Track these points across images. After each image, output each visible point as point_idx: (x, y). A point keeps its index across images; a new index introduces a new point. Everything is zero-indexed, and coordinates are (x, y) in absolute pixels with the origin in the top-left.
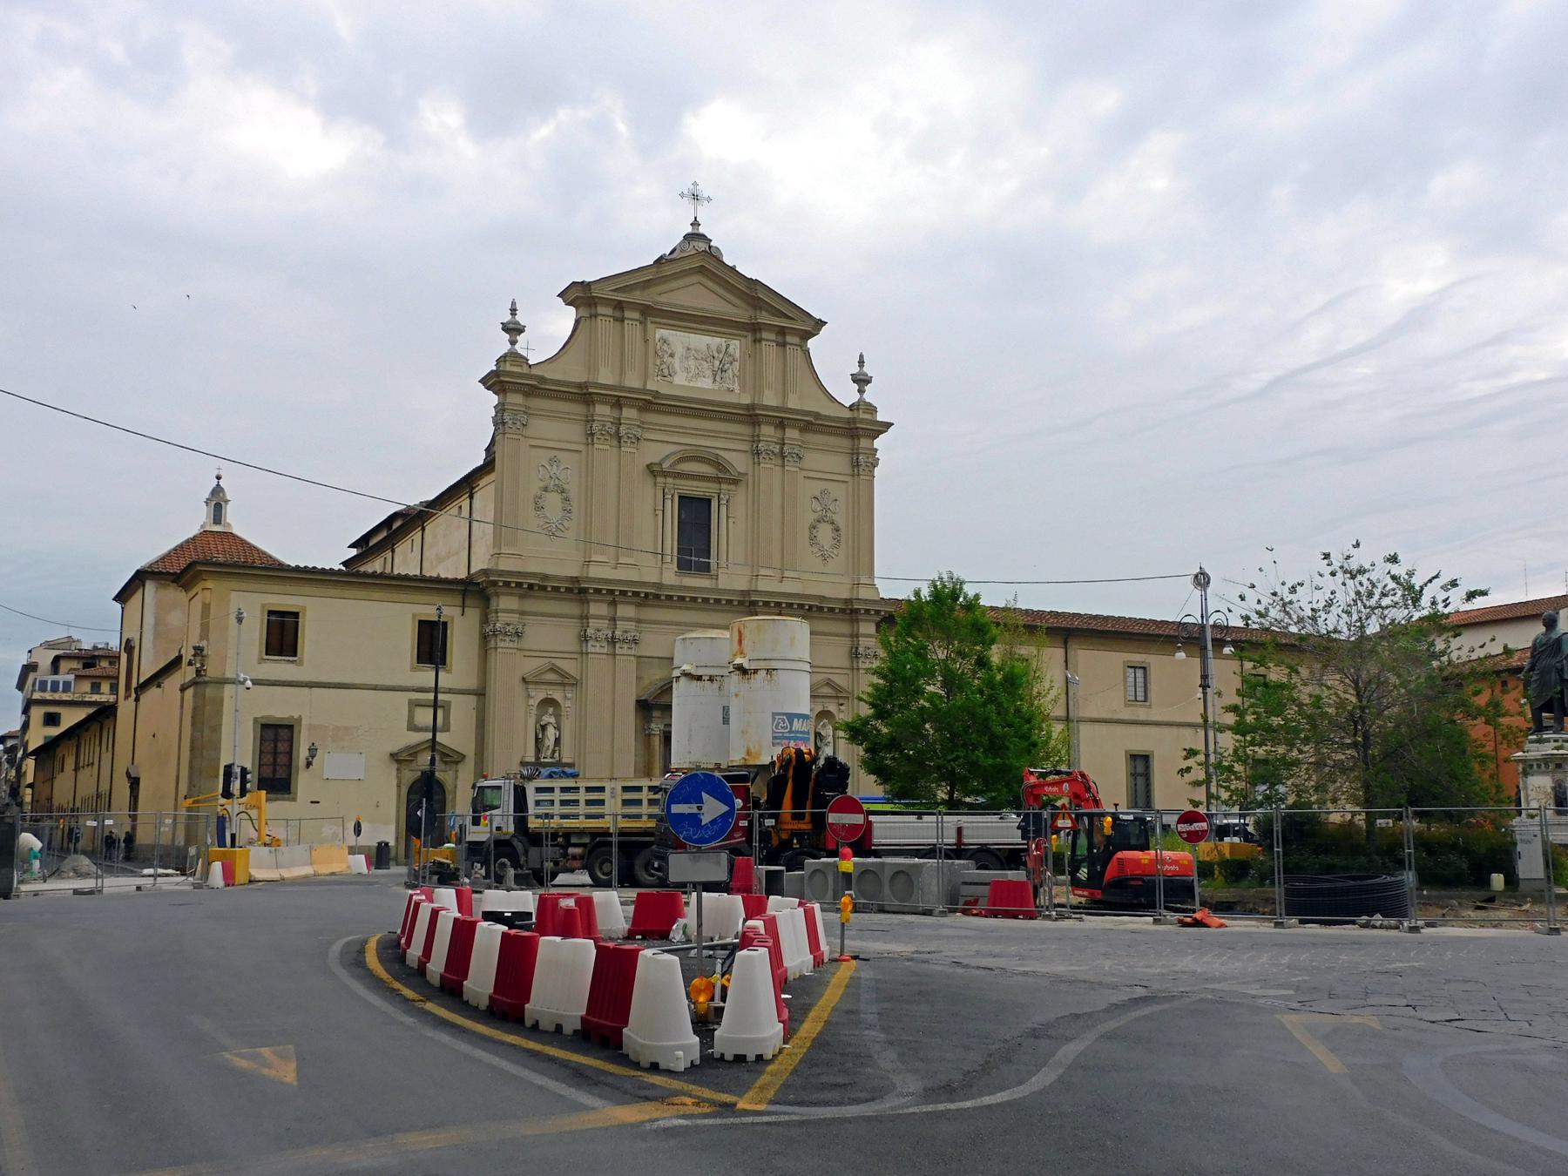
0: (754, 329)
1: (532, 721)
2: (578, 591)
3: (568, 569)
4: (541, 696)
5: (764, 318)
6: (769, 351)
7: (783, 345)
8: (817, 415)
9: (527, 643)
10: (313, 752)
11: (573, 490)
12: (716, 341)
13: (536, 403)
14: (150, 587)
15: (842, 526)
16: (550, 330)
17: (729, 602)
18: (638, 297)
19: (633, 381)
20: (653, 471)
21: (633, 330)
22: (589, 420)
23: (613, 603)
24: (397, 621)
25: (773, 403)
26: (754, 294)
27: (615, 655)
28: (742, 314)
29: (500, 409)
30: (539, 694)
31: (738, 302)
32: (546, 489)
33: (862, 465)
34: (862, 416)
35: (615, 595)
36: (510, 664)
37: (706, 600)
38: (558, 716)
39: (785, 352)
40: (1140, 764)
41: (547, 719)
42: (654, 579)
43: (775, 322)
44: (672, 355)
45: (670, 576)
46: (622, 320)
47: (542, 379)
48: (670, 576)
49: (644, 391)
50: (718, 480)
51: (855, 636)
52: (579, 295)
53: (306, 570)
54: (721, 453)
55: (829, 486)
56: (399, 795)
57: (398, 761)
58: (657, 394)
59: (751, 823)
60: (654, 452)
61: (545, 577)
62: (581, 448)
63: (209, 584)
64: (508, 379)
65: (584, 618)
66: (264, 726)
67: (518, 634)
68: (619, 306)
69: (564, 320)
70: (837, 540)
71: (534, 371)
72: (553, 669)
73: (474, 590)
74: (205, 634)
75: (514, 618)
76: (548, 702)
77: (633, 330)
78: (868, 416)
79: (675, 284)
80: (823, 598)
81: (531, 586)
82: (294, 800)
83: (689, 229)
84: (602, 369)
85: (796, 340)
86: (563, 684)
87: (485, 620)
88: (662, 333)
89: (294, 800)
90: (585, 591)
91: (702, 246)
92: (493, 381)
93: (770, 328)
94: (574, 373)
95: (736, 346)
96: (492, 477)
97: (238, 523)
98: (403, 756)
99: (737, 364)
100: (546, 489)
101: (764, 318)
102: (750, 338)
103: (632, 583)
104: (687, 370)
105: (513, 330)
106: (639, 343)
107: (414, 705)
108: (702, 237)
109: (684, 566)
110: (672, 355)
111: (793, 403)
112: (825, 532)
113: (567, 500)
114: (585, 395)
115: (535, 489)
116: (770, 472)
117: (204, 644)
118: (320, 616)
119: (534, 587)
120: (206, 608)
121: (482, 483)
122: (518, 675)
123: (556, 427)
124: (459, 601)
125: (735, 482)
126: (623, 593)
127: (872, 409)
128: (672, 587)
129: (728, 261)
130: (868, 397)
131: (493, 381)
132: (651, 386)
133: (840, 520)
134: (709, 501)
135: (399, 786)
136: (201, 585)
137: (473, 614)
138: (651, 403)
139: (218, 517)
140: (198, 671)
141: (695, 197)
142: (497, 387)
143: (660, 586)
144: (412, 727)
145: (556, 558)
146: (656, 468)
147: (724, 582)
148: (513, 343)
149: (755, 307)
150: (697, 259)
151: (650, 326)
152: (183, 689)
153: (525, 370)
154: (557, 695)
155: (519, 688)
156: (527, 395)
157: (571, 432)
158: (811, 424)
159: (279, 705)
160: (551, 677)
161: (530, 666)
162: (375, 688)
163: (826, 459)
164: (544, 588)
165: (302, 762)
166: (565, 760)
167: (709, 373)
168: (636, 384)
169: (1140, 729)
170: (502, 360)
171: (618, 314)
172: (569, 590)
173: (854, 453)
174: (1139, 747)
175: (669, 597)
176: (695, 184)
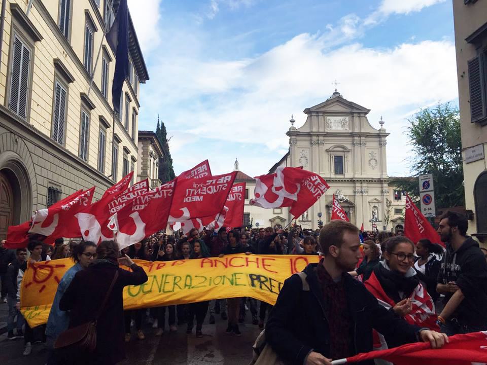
0: (352, 113)
4: (373, 206)
5: (355, 111)
6: (356, 119)
7: (360, 117)
8: (369, 133)
9: (370, 193)
11: (308, 157)
13: (298, 138)
15: (378, 160)
16: (301, 121)
17: (348, 181)
18: (322, 110)
19: (321, 130)
20: (327, 151)
21: (321, 118)
22: (311, 140)
25: (358, 131)
26: (351, 105)
28: (348, 110)
29: (290, 140)
30: (372, 205)
31: (346, 107)
32: (302, 157)
33: (382, 144)
34: (382, 132)
35: (362, 181)
37: (342, 181)
39: (318, 118)
42: (329, 177)
43: (356, 111)
46: (318, 116)
47: (299, 132)
48: (333, 176)
49: (324, 132)
50: (344, 151)
51: (382, 187)
52: (307, 111)
54: (345, 145)
55: (373, 150)
57: (271, 221)
58: (327, 133)
60: (327, 147)
64: (292, 134)
65: (355, 187)
67: (367, 192)
68: (317, 112)
70: (377, 164)
71: (298, 131)
72: (376, 199)
75: (366, 188)
76: (375, 207)
77: (321, 118)
78: (384, 132)
79: (330, 106)
80: (373, 178)
81: (369, 181)
83: (335, 92)
84: (355, 129)
85: (363, 115)
88: (328, 118)
91: (338, 95)
92: (289, 134)
93: (355, 113)
94: (307, 130)
95: (347, 119)
96: (289, 156)
97: (241, 169)
99: (348, 123)
100: (302, 157)
101: (355, 111)
103: (360, 178)
104: (335, 126)
105: (292, 121)
106: (323, 121)
108: (338, 93)
109: (336, 173)
111: (363, 131)
112: (373, 162)
114: (310, 135)
115: (369, 159)
116: (357, 148)
122: (368, 201)
123: (304, 143)
125: (349, 152)
126: (364, 181)
127: (385, 130)
128: (334, 178)
129: (344, 98)
131: (289, 134)
132: (326, 131)
133: (377, 158)
134: (342, 157)
138: (326, 135)
139: (237, 169)
141: (336, 83)
143: (330, 178)
144: (274, 213)
148: (293, 124)
149: (352, 108)
153: (296, 131)
154: (377, 205)
155: (368, 204)
156: (366, 137)
157: (307, 144)
158: (368, 135)
160: (376, 201)
161: (370, 199)
163: (373, 144)
168: (322, 131)
170: (290, 129)
171: (317, 115)
172: (351, 181)
173: (380, 141)
175: (333, 181)
176: (336, 80)
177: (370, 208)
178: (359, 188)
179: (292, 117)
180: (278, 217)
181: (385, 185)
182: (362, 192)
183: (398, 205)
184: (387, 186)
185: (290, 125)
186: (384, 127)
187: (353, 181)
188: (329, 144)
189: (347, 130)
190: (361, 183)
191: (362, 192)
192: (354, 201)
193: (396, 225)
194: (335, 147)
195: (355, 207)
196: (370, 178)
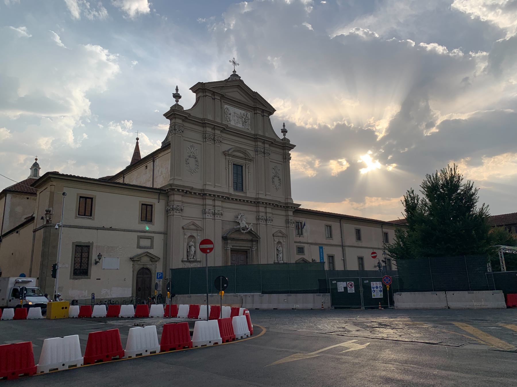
0: (255, 109)
1: (186, 244)
2: (203, 194)
3: (198, 186)
6: (259, 117)
7: (214, 99)
10: (100, 256)
12: (243, 112)
14: (9, 196)
16: (188, 101)
17: (251, 202)
20: (225, 154)
23: (214, 200)
24: (133, 203)
27: (215, 219)
28: (251, 103)
35: (215, 196)
36: (178, 221)
38: (195, 242)
40: (361, 259)
41: (191, 243)
44: (230, 114)
45: (232, 191)
46: (214, 99)
49: (222, 124)
53: (82, 178)
54: (248, 151)
55: (193, 144)
56: (133, 275)
59: (223, 286)
61: (192, 188)
62: (202, 143)
63: (54, 183)
64: (175, 114)
66: (77, 246)
67: (182, 210)
68: (214, 93)
69: (193, 97)
73: (164, 193)
74: (51, 203)
75: (180, 204)
76: (279, 242)
77: (218, 102)
82: (90, 278)
86: (197, 230)
87: (167, 204)
88: (226, 106)
89: (90, 278)
90: (205, 194)
96: (169, 150)
98: (136, 259)
102: (253, 112)
107: (139, 238)
109: (236, 189)
110: (230, 114)
112: (276, 180)
113: (197, 161)
117: (51, 209)
118: (102, 198)
119: (187, 192)
120: (52, 194)
121: (160, 155)
123: (193, 134)
124: (157, 197)
125: (250, 160)
127: (288, 141)
130: (286, 137)
135: (133, 271)
136: (51, 183)
137: (163, 202)
140: (47, 221)
142: (172, 116)
144: (139, 247)
145: (194, 181)
146: (226, 153)
147: (248, 195)
148: (177, 101)
150: (235, 82)
151: (223, 103)
152: (35, 231)
154: (195, 235)
155: (182, 230)
156: (183, 121)
159: (84, 237)
160: (193, 227)
161: (185, 222)
162: (124, 230)
163: (276, 156)
164: (191, 193)
165: (93, 261)
166: (198, 260)
167: (241, 122)
169: (355, 249)
174: (360, 255)
176: (234, 58)
177: (274, 244)
178: (263, 214)
179: (177, 90)
180: (147, 254)
181: (290, 213)
182: (266, 220)
183: (300, 242)
184: (292, 214)
185: (173, 102)
186: (287, 137)
187: (257, 203)
188: (228, 144)
189: (248, 128)
190: (214, 200)
191: (266, 220)
192: (257, 231)
193: (138, 267)
194: (234, 151)
195: (257, 241)
196: (188, 187)
